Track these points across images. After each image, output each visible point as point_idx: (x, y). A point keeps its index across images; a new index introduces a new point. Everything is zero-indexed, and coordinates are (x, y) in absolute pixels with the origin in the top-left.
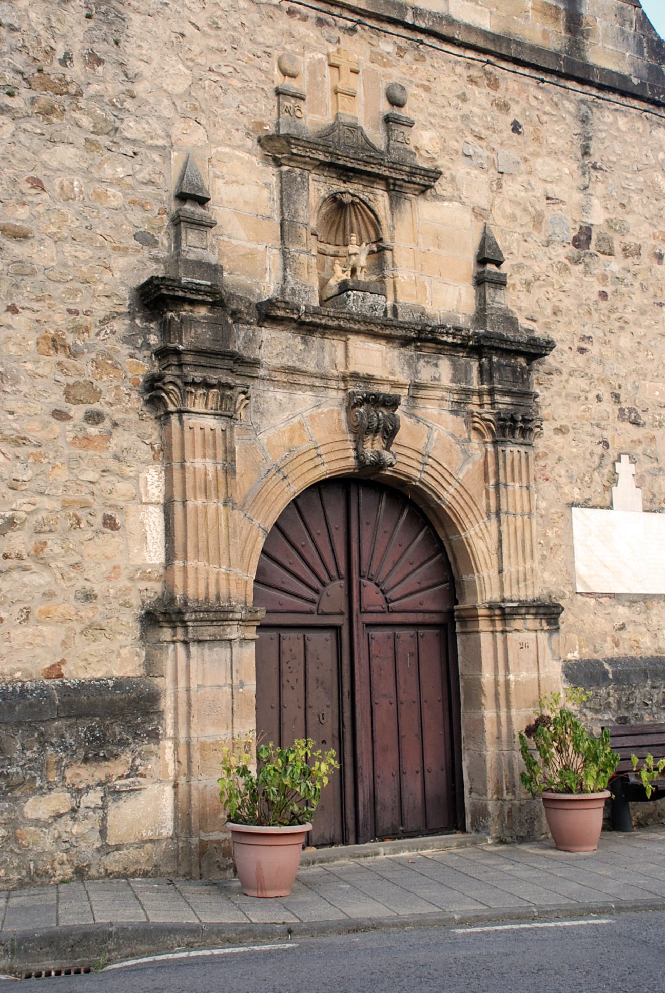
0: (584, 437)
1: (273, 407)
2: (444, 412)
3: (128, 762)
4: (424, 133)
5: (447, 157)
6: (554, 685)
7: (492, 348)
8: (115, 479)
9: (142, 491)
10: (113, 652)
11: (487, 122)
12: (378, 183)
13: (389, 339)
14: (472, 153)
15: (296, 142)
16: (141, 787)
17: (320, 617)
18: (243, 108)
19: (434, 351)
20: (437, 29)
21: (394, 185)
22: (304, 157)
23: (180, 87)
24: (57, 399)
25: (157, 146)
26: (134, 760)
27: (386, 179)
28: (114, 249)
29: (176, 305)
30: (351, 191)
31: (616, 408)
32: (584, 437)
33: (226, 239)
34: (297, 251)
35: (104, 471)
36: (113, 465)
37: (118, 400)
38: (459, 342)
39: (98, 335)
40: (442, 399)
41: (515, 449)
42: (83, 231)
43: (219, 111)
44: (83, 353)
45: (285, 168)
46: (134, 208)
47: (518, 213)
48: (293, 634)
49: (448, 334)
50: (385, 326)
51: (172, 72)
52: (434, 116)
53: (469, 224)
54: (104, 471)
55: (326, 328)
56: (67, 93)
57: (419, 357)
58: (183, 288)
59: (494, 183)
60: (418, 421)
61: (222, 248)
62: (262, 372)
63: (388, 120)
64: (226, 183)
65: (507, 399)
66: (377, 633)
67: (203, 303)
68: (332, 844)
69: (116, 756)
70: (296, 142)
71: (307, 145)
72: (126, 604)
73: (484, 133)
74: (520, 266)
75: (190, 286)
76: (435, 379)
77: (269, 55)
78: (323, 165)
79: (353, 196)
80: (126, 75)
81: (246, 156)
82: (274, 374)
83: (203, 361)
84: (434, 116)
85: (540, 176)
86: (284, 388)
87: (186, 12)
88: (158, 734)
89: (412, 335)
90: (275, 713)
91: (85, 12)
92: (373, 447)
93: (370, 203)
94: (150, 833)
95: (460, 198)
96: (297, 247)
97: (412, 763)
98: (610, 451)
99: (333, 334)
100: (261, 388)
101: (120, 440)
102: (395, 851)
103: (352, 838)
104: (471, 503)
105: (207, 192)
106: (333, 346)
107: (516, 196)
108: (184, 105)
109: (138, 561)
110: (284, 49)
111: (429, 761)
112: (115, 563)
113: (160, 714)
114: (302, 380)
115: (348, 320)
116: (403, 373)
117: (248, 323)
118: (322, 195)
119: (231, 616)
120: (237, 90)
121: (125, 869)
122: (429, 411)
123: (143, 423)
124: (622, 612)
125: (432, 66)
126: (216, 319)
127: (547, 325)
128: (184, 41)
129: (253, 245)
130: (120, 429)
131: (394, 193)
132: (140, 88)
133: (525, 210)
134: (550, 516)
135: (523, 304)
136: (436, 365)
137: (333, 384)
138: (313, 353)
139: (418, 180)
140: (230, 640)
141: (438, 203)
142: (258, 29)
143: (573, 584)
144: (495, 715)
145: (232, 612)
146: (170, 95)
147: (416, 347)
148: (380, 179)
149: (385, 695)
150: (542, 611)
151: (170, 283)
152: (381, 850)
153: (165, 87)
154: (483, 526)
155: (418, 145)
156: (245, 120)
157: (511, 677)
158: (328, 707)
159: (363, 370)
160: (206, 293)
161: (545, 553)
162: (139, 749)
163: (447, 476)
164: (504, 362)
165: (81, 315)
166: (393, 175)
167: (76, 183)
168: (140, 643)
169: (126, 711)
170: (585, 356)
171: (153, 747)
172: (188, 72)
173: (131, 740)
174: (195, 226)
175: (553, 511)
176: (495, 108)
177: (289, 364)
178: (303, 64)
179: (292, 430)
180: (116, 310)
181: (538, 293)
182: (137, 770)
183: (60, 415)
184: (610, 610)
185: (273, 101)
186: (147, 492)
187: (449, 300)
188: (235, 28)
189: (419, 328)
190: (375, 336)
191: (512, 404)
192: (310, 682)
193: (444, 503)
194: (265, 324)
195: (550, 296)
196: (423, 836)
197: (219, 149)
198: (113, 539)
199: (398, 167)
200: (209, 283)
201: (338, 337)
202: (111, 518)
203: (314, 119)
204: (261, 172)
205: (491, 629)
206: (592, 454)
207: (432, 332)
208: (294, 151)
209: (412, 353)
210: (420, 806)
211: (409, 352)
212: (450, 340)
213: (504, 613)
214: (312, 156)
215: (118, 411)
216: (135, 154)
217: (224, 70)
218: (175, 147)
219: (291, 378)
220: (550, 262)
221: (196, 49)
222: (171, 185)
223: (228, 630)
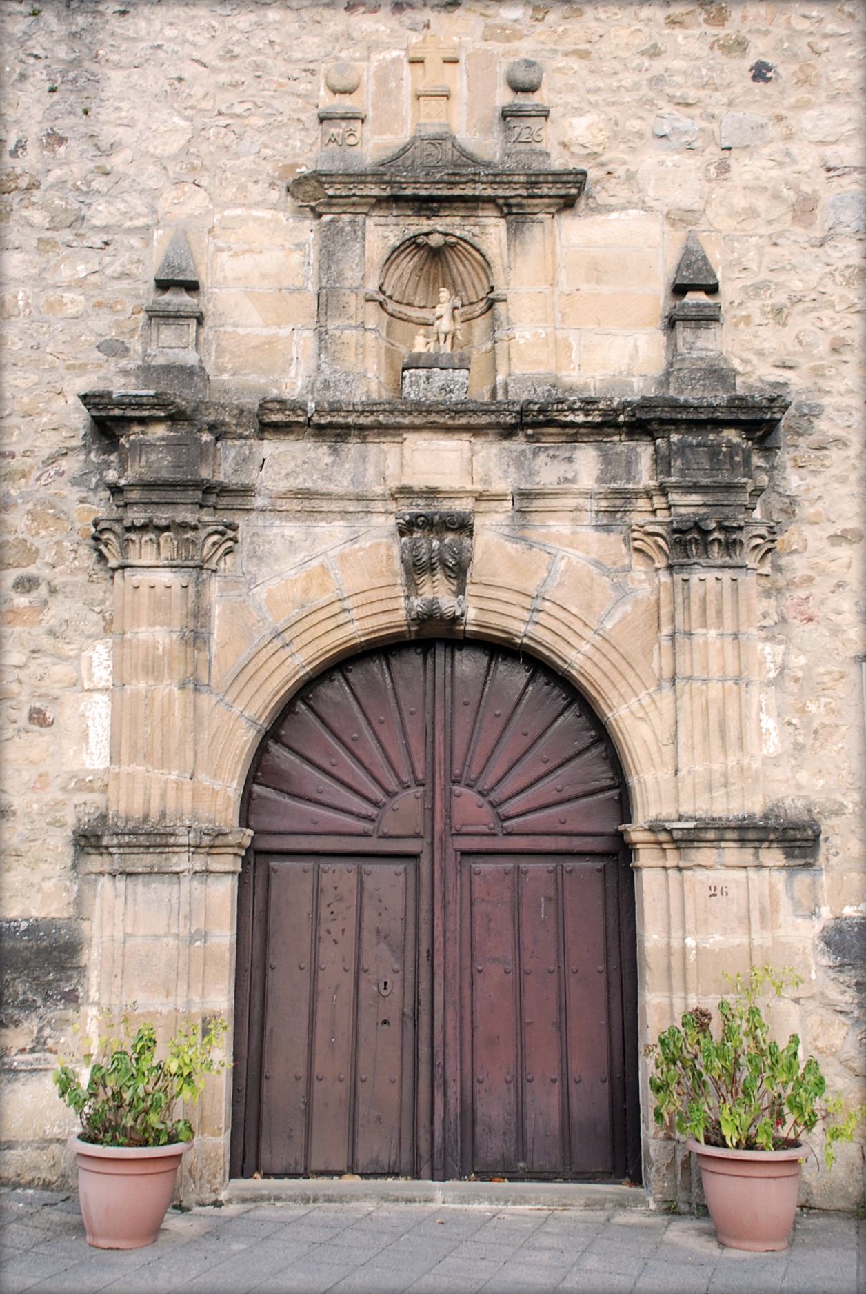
1: (280, 547)
2: (583, 530)
3: (32, 1032)
4: (575, 121)
5: (622, 146)
6: (798, 959)
7: (662, 422)
8: (48, 660)
9: (84, 674)
10: (32, 885)
11: (701, 77)
12: (483, 209)
13: (475, 430)
14: (667, 131)
15: (330, 179)
16: (49, 1066)
17: (382, 840)
18: (267, 152)
19: (564, 439)
21: (509, 206)
22: (348, 197)
23: (174, 144)
25: (137, 228)
26: (41, 1030)
27: (491, 200)
28: (68, 368)
29: (123, 427)
30: (440, 229)
33: (229, 329)
34: (338, 328)
35: (34, 652)
36: (46, 642)
37: (61, 558)
38: (598, 419)
39: (38, 479)
40: (578, 509)
41: (710, 576)
42: (28, 352)
43: (229, 163)
44: (15, 505)
45: (326, 218)
46: (100, 312)
47: (761, 203)
48: (340, 865)
49: (572, 410)
50: (456, 412)
51: (162, 129)
52: (597, 90)
53: (658, 238)
54: (34, 652)
55: (361, 428)
56: (16, 188)
57: (535, 454)
58: (118, 404)
59: (712, 168)
60: (531, 547)
61: (224, 343)
62: (259, 502)
63: (507, 115)
64: (235, 255)
65: (695, 498)
66: (485, 866)
67: (159, 420)
68: (396, 1174)
69: (17, 1023)
70: (330, 179)
71: (347, 179)
72: (57, 823)
73: (692, 94)
74: (760, 288)
75: (127, 401)
76: (566, 480)
77: (313, 72)
78: (380, 202)
79: (446, 234)
80: (98, 148)
81: (267, 214)
82: (279, 502)
83: (155, 497)
84: (597, 90)
85: (812, 138)
86: (298, 519)
87: (188, 49)
88: (77, 997)
89: (510, 420)
90: (305, 976)
91: (48, 85)
93: (475, 241)
94: (56, 1130)
95: (644, 202)
96: (338, 322)
97: (544, 1063)
99: (379, 435)
100: (260, 523)
101: (59, 610)
102: (463, 1200)
103: (425, 1170)
104: (623, 666)
105: (195, 273)
106: (382, 452)
107: (758, 179)
108: (178, 169)
109: (74, 766)
110: (337, 59)
111: (577, 1066)
112: (42, 770)
113: (81, 970)
114: (325, 506)
115: (391, 412)
116: (506, 478)
117: (241, 437)
118: (390, 243)
119: (172, 840)
120: (259, 130)
121: (19, 1175)
122: (554, 530)
123: (93, 586)
125: (598, 20)
126: (180, 438)
127: (818, 372)
128: (181, 87)
129: (273, 331)
130: (60, 596)
131: (511, 218)
132: (117, 162)
133: (776, 196)
134: (818, 679)
135: (766, 345)
136: (570, 460)
137: (379, 506)
138: (347, 466)
139: (545, 191)
140: (177, 873)
141: (599, 218)
142: (295, 42)
144: (666, 1001)
145: (172, 835)
146: (158, 160)
147: (528, 436)
148: (484, 202)
149: (495, 960)
150: (751, 835)
151: (97, 400)
152: (439, 1195)
153: (151, 150)
154: (646, 701)
155: (565, 140)
156: (269, 167)
157: (690, 942)
158: (396, 972)
159: (418, 483)
160: (153, 406)
161: (800, 739)
162: (49, 1016)
163: (577, 626)
164: (692, 440)
165: (18, 457)
166: (500, 192)
167: (20, 295)
168: (72, 874)
169: (32, 964)
171: (71, 1014)
172: (183, 123)
173: (39, 1003)
174: (171, 321)
175: (821, 670)
176: (718, 52)
177: (307, 485)
178: (367, 72)
179: (309, 576)
180: (66, 445)
181: (800, 322)
182: (45, 1043)
185: (316, 131)
186: (91, 676)
187: (621, 356)
188: (259, 51)
189: (518, 408)
190: (448, 429)
191: (704, 505)
192: (367, 936)
193: (573, 668)
194: (267, 435)
195: (826, 323)
196: (565, 1180)
197: (226, 213)
198: (41, 739)
199: (505, 179)
200: (152, 392)
201: (389, 439)
202: (39, 711)
203: (373, 145)
204: (293, 229)
205: (661, 863)
207: (540, 411)
208: (330, 192)
209: (525, 446)
210: (557, 1133)
211: (519, 444)
212: (580, 418)
213: (685, 838)
214: (359, 193)
215: (61, 573)
216: (106, 243)
217: (239, 109)
218: (162, 223)
219: (307, 505)
220: (828, 269)
221: (198, 91)
222: (151, 271)
223: (175, 859)
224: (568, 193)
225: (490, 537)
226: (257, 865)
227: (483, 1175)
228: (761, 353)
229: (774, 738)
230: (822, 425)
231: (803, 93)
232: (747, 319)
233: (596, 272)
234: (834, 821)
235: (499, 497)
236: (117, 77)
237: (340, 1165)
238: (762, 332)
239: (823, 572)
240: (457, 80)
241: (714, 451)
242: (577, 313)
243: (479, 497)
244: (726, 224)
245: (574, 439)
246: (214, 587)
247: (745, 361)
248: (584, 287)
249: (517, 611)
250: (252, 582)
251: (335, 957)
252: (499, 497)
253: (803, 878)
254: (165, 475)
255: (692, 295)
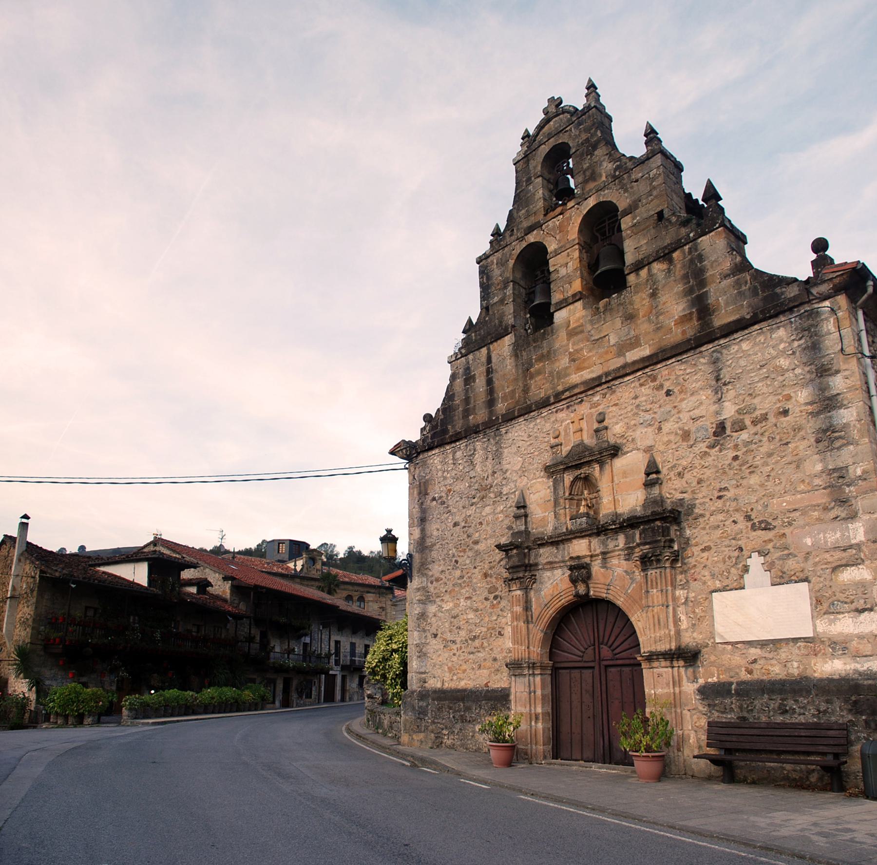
0: (723, 549)
1: (546, 579)
13: (590, 536)
20: (618, 375)
24: (486, 594)
31: (749, 524)
32: (723, 549)
40: (619, 555)
41: (653, 572)
47: (672, 437)
62: (540, 567)
63: (597, 431)
65: (647, 547)
66: (613, 670)
73: (648, 407)
78: (565, 470)
92: (582, 589)
98: (744, 553)
124: (754, 652)
133: (676, 434)
143: (714, 638)
159: (574, 555)
170: (722, 500)
181: (687, 476)
183: (486, 599)
184: (744, 651)
192: (584, 692)
195: (695, 474)
206: (730, 558)
211: (602, 537)
213: (652, 657)
224: (615, 451)
225: (596, 568)
226: (555, 671)
227: (616, 764)
228: (675, 489)
229: (685, 622)
230: (696, 511)
231: (683, 396)
232: (670, 479)
233: (625, 474)
234: (706, 649)
235: (597, 555)
236: (506, 451)
237: (579, 758)
238: (675, 482)
239: (699, 563)
240: (584, 424)
241: (653, 529)
242: (621, 492)
243: (591, 556)
244: (662, 448)
245: (617, 533)
246: (532, 593)
247: (670, 494)
248: (622, 480)
249: (603, 590)
250: (541, 590)
251: (576, 698)
252: (597, 555)
253: (690, 670)
254: (517, 564)
255: (653, 474)
